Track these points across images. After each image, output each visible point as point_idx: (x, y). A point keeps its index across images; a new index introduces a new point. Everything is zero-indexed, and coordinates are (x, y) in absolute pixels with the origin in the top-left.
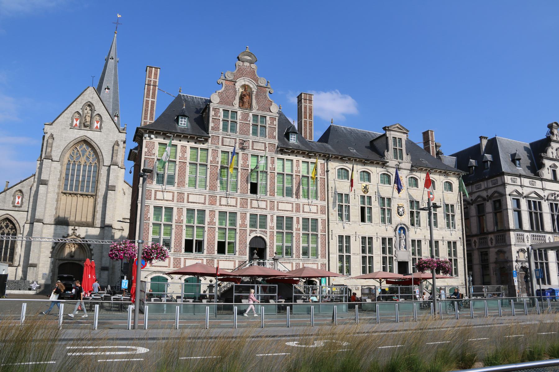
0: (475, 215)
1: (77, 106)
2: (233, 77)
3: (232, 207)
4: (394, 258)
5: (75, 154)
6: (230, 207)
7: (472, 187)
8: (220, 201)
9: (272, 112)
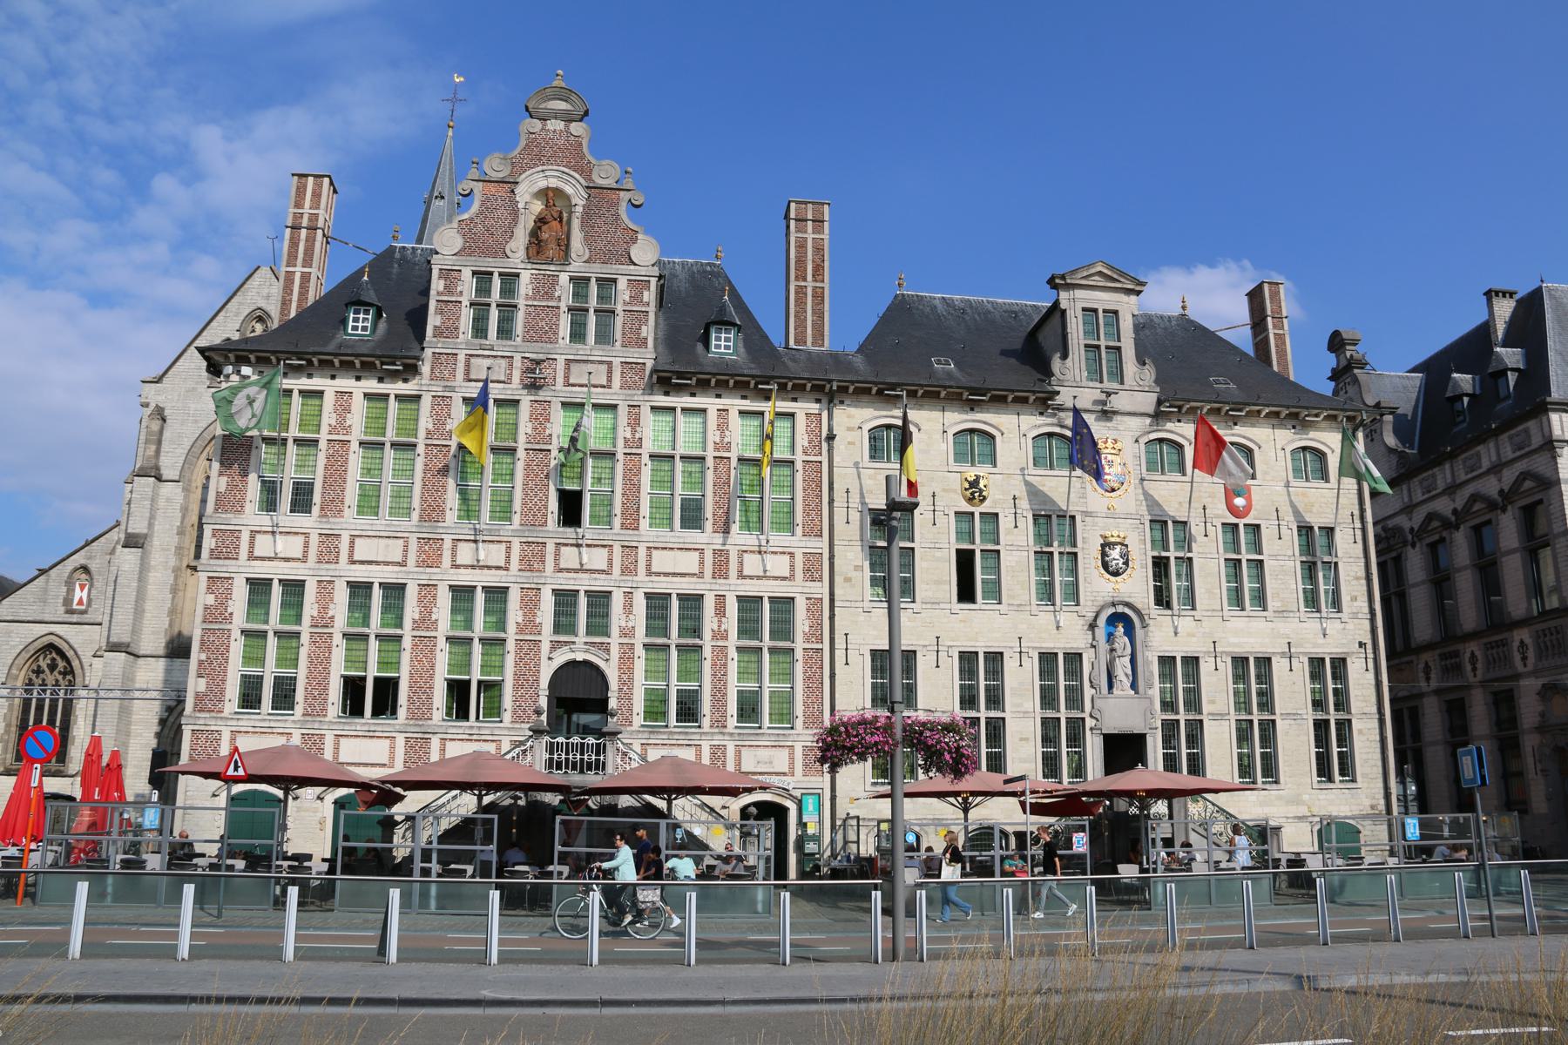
0: (1468, 562)
2: (510, 168)
3: (493, 571)
4: (1089, 723)
6: (486, 571)
7: (1452, 466)
8: (454, 555)
9: (635, 265)
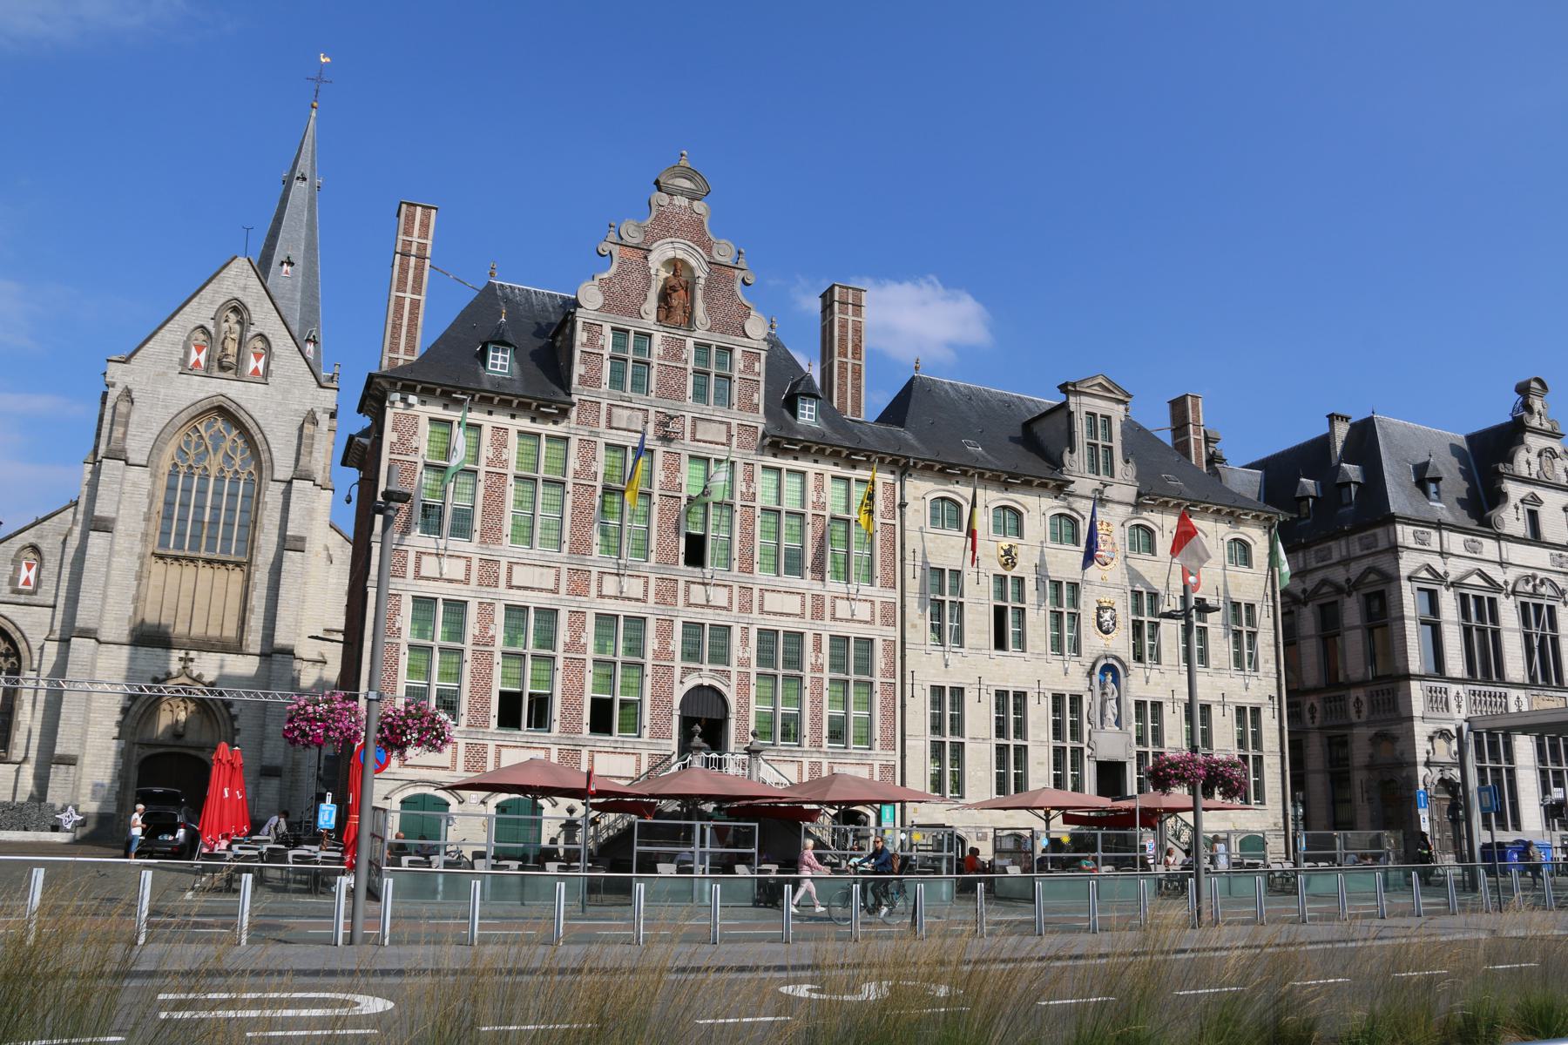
0: (1313, 633)
1: (201, 311)
2: (643, 236)
3: (633, 603)
4: (1087, 752)
5: (193, 445)
6: (627, 602)
7: (1304, 556)
8: (600, 585)
9: (748, 337)
